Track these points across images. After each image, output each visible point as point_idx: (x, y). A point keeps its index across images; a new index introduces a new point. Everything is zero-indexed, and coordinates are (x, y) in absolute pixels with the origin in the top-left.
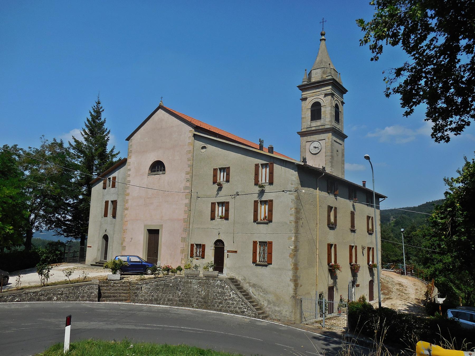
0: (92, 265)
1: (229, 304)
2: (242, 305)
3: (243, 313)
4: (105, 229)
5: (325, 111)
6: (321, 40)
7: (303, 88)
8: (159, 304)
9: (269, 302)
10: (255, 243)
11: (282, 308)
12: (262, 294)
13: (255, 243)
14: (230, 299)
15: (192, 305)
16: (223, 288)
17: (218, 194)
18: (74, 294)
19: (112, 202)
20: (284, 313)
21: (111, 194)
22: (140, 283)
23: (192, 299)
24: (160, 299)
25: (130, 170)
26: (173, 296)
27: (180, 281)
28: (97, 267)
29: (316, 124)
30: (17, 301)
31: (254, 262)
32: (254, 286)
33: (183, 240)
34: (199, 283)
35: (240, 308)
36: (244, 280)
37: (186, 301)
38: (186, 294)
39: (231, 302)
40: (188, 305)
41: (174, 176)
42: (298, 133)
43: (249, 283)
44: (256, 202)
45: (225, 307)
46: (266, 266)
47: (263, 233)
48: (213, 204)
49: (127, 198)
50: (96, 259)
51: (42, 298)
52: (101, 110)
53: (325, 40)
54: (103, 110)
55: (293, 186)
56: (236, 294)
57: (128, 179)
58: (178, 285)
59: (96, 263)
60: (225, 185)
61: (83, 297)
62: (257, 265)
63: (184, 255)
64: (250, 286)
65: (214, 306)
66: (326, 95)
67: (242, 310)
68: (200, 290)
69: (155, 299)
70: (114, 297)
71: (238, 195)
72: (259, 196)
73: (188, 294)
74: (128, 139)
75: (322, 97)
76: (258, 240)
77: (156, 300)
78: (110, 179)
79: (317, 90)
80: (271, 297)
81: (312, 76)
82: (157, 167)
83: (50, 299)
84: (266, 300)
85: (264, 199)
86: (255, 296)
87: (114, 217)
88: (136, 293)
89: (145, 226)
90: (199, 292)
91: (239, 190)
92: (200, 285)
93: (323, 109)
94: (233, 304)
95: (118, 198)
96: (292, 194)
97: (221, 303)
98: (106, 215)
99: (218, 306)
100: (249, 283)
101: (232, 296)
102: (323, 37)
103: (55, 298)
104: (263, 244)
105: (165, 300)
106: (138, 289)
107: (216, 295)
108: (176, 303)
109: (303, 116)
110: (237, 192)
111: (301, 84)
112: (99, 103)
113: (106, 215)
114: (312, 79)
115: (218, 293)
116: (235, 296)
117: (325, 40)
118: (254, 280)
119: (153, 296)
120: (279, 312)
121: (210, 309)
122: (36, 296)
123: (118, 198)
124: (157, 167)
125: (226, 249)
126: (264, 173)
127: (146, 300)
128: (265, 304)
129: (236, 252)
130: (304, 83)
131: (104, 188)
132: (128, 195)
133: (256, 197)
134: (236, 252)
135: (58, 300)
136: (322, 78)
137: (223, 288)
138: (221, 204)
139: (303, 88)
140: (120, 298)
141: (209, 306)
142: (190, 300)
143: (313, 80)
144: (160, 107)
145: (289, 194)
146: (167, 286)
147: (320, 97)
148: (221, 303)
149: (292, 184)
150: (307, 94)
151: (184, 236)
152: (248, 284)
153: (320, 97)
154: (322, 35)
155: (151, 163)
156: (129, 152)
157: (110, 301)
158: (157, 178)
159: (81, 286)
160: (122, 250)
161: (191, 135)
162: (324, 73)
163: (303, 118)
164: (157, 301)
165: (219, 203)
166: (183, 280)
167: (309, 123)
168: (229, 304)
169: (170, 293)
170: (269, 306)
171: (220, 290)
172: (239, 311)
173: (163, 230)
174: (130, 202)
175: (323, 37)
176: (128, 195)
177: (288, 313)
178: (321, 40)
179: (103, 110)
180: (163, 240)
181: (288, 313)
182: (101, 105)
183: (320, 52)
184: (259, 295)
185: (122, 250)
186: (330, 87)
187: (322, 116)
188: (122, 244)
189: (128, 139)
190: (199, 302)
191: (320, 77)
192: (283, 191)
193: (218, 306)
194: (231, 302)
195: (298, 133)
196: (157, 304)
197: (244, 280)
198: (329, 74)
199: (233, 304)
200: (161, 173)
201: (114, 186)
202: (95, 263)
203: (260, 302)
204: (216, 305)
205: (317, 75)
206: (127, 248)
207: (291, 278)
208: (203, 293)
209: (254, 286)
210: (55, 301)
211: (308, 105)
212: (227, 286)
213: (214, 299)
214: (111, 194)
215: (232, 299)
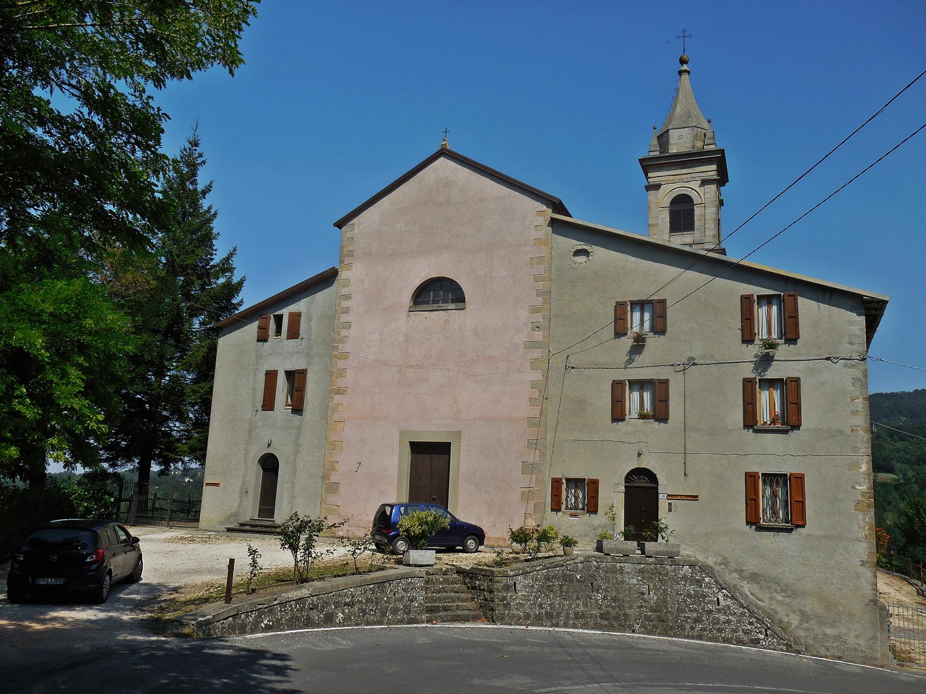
0: (229, 530)
1: (718, 623)
2: (751, 624)
3: (755, 642)
4: (266, 441)
6: (680, 73)
7: (647, 165)
8: (557, 625)
9: (805, 616)
10: (751, 478)
11: (843, 630)
12: (780, 598)
13: (751, 478)
14: (719, 611)
15: (630, 626)
16: (699, 583)
17: (630, 361)
18: (377, 605)
19: (290, 374)
20: (851, 641)
21: (283, 355)
22: (512, 573)
23: (629, 612)
24: (558, 615)
25: (348, 297)
26: (586, 606)
27: (598, 568)
28: (250, 535)
29: (678, 241)
30: (268, 628)
31: (752, 520)
32: (754, 578)
33: (529, 468)
34: (641, 571)
35: (746, 632)
36: (722, 564)
37: (616, 618)
38: (614, 599)
39: (722, 618)
40: (623, 628)
41: (498, 314)
43: (740, 571)
44: (748, 384)
45: (710, 631)
46: (789, 531)
47: (774, 454)
48: (617, 386)
49: (340, 364)
50: (236, 515)
51: (314, 615)
52: (200, 160)
53: (689, 72)
54: (204, 162)
55: (855, 347)
56: (733, 597)
57: (344, 318)
58: (593, 576)
59: (241, 525)
60: (653, 342)
61: (395, 611)
62: (760, 529)
63: (531, 504)
64: (742, 578)
65: (682, 628)
66: (704, 182)
67: (754, 636)
68: (644, 589)
69: (547, 613)
70: (446, 609)
71: (695, 364)
72: (756, 369)
73: (618, 600)
74: (340, 225)
75: (695, 185)
76: (761, 470)
77: (549, 616)
78: (279, 319)
79: (684, 171)
80: (811, 605)
81: (671, 142)
82: (438, 292)
83: (329, 619)
84: (794, 612)
85: (771, 374)
86: (760, 603)
87: (298, 409)
88: (504, 598)
89: (402, 434)
90: (643, 594)
91: (696, 353)
92: (643, 578)
93: (697, 211)
94: (728, 622)
95: (309, 364)
96: (853, 366)
97: (698, 620)
98: (268, 404)
99: (692, 628)
100: (740, 571)
101: (722, 603)
102: (685, 67)
103: (340, 615)
104: (772, 479)
105: (568, 615)
106: (507, 588)
107: (685, 601)
108: (595, 624)
110: (691, 359)
111: (645, 155)
112: (195, 144)
113: (268, 404)
115: (689, 596)
116: (729, 602)
117: (689, 72)
118: (753, 565)
119: (541, 606)
120: (838, 638)
121: (676, 635)
122: (302, 609)
123: (309, 364)
124: (438, 292)
125: (664, 490)
126: (766, 318)
127: (527, 617)
128: (794, 620)
129: (695, 498)
130: (652, 154)
131: (262, 338)
132: (345, 356)
133: (748, 371)
134: (695, 498)
135: (347, 620)
136: (693, 147)
137: (699, 583)
138: (640, 385)
139: (647, 165)
140: (459, 612)
141: (671, 629)
142: (625, 615)
143: (673, 150)
144: (444, 153)
145: (845, 366)
146: (567, 578)
147: (691, 185)
148: (698, 620)
149: (851, 343)
150: (656, 176)
151: (530, 460)
152: (735, 575)
153: (691, 185)
154: (683, 62)
155: (418, 282)
156: (344, 255)
157: (443, 621)
158: (433, 319)
159: (389, 581)
160: (327, 491)
161: (543, 221)
162: (696, 137)
163: (653, 225)
164: (550, 618)
165: (632, 383)
166: (604, 564)
167: (666, 236)
168: (718, 623)
169: (578, 599)
170: (805, 625)
171: (692, 589)
172: (745, 638)
173: (463, 444)
174: (350, 375)
175: (685, 67)
176: (345, 356)
177: (862, 642)
178: (680, 73)
179: (204, 162)
180: (463, 468)
181: (862, 642)
182: (199, 150)
183: (681, 96)
184: (772, 598)
185: (327, 491)
186: (714, 167)
187: (697, 223)
188: (325, 477)
189: (340, 225)
190: (647, 618)
191: (689, 145)
192: (828, 359)
193: (692, 628)
194: (722, 618)
196: (553, 625)
197: (722, 564)
198: (711, 141)
199: (728, 622)
200: (452, 306)
201: (294, 333)
202: (238, 527)
203: (777, 617)
204: (688, 626)
205: (681, 141)
206: (342, 488)
207: (865, 558)
208: (653, 597)
209: (754, 578)
210: (339, 625)
211: (663, 198)
212: (707, 579)
213: (680, 610)
214: (283, 355)
215: (726, 610)
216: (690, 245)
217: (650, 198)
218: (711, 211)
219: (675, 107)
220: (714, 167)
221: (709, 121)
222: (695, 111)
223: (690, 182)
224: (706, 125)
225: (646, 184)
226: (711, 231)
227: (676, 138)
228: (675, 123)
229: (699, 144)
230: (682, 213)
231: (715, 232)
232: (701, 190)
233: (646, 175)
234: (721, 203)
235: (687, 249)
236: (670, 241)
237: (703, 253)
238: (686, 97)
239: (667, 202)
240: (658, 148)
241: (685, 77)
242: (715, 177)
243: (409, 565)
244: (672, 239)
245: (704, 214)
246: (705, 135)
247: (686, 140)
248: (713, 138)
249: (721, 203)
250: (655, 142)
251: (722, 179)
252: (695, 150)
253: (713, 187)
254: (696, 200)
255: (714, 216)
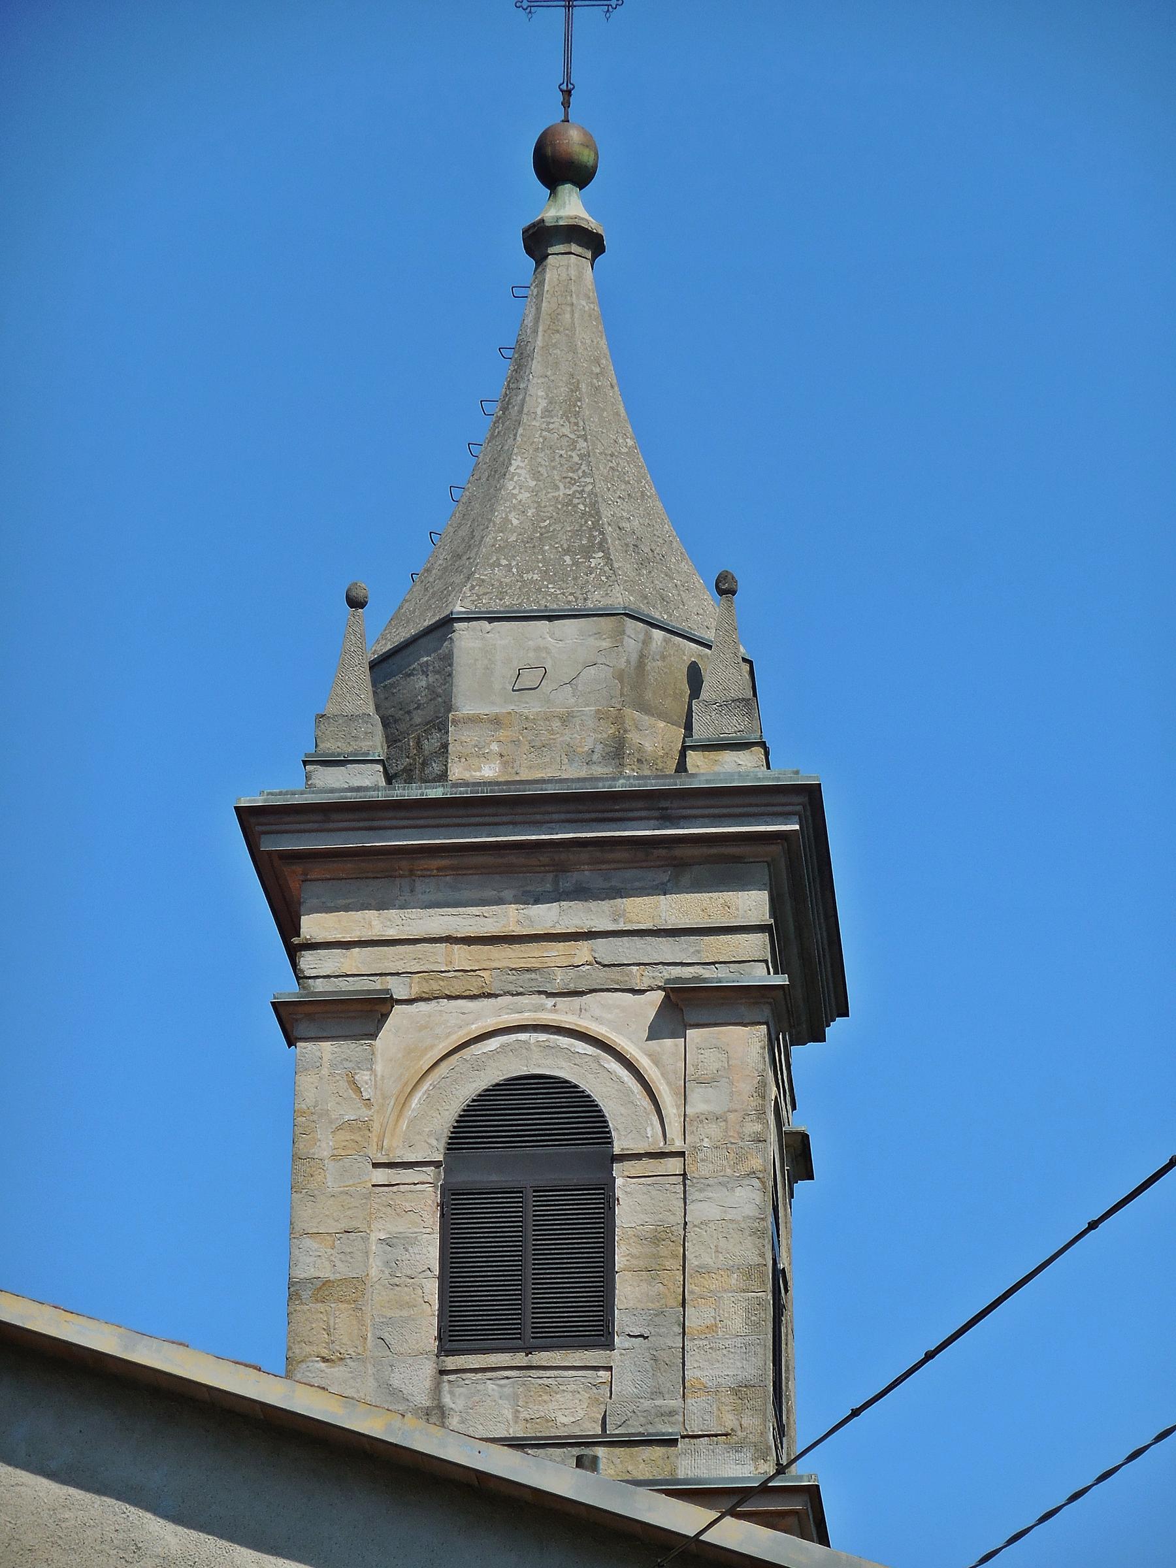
5: (672, 1240)
6: (539, 240)
7: (299, 856)
42: (823, 1539)
53: (593, 243)
66: (685, 1006)
75: (625, 1018)
79: (509, 917)
81: (466, 705)
93: (635, 1203)
102: (570, 206)
109: (314, 1262)
111: (284, 784)
114: (460, 738)
117: (593, 243)
136: (617, 751)
143: (477, 764)
150: (350, 939)
154: (556, 168)
162: (634, 684)
163: (323, 1289)
167: (417, 1378)
175: (570, 206)
178: (539, 240)
186: (752, 904)
187: (629, 1292)
191: (589, 737)
195: (823, 1539)
198: (733, 726)
205: (531, 706)
211: (403, 1092)
216: (582, 1450)
217: (309, 1087)
218: (729, 1206)
219: (498, 470)
220: (752, 904)
221: (725, 588)
222: (633, 507)
223: (580, 994)
224: (702, 611)
225: (289, 989)
226: (726, 1355)
227: (503, 676)
228: (495, 579)
229: (656, 738)
230: (528, 1220)
231: (758, 1365)
232: (660, 1059)
233: (288, 925)
234: (798, 1157)
235: (555, 1477)
236: (437, 1413)
237: (685, 1519)
238: (572, 410)
239: (427, 1128)
240: (375, 743)
241: (566, 264)
242: (760, 975)
243: (496, 996)
244: (455, 1398)
245: (683, 1223)
246: (695, 677)
247: (565, 699)
248: (749, 703)
249: (798, 1157)
250: (360, 698)
251: (805, 996)
252: (628, 779)
253: (746, 1042)
254: (629, 1127)
255: (749, 1251)
